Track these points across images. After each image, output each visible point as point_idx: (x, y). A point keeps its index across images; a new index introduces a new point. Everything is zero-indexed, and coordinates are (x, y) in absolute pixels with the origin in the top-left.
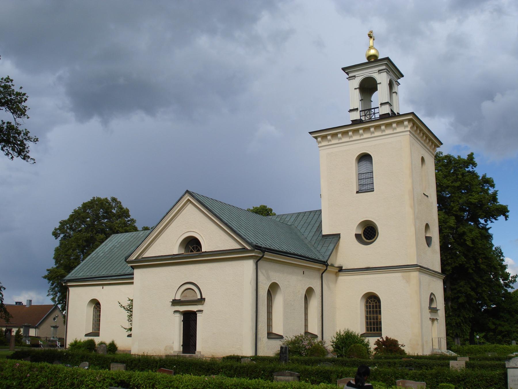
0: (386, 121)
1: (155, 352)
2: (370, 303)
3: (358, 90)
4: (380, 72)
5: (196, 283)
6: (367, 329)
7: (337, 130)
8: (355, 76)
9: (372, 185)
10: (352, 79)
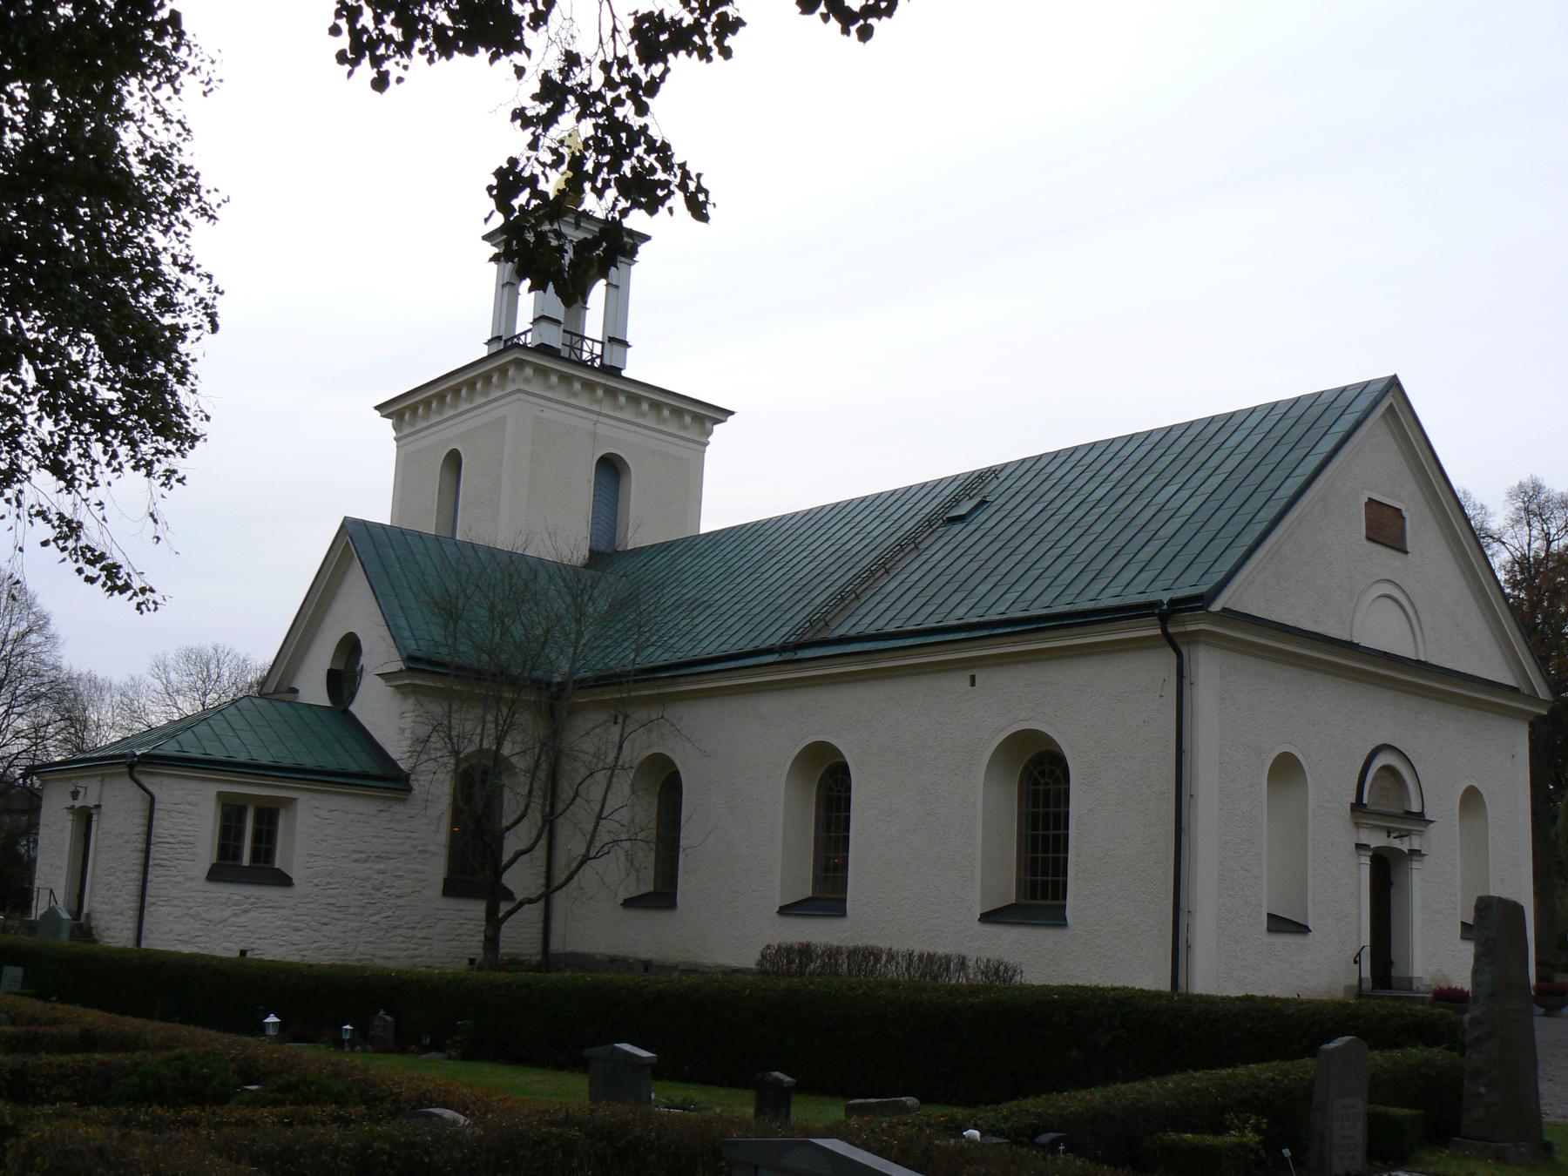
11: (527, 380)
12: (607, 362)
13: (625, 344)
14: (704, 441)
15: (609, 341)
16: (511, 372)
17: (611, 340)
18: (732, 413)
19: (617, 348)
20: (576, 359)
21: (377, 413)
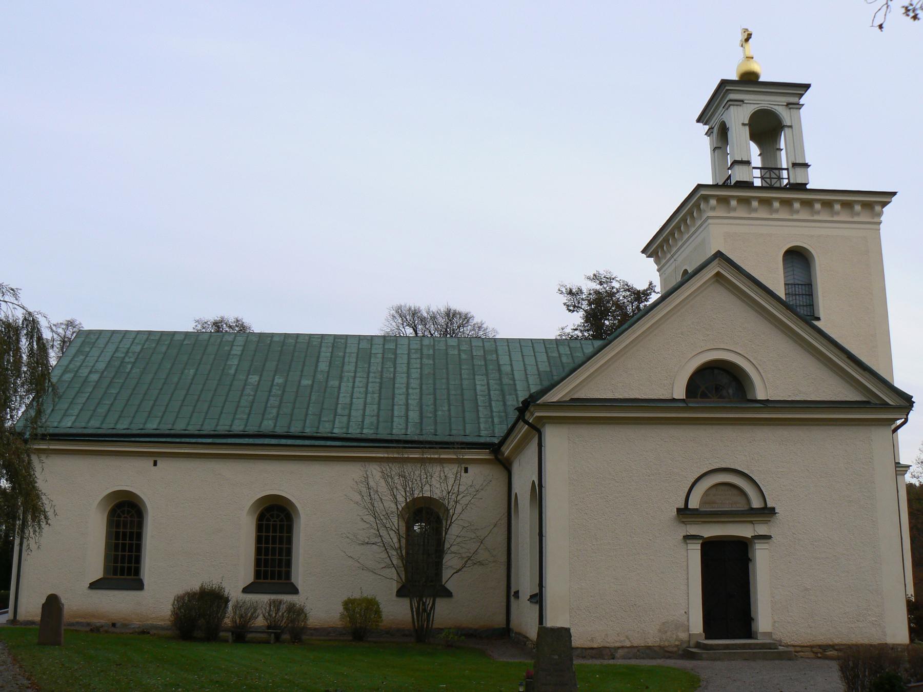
0: (862, 197)
1: (627, 637)
2: (268, 520)
3: (747, 128)
4: (791, 106)
5: (746, 472)
6: (258, 574)
7: (769, 193)
8: (742, 101)
9: (812, 307)
10: (737, 105)
11: (713, 209)
12: (792, 181)
13: (806, 165)
14: (875, 220)
15: (793, 166)
16: (702, 206)
17: (795, 165)
18: (894, 194)
19: (799, 170)
20: (768, 186)
21: (644, 255)
